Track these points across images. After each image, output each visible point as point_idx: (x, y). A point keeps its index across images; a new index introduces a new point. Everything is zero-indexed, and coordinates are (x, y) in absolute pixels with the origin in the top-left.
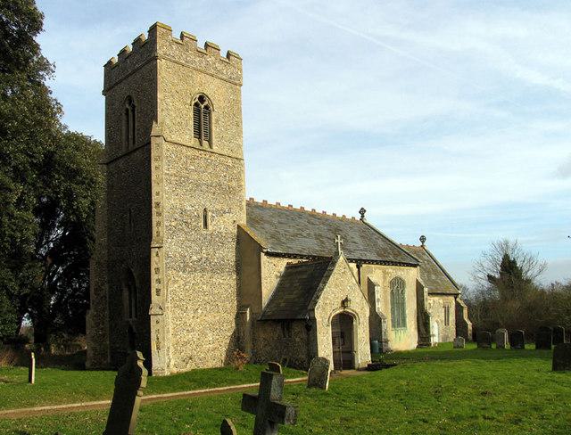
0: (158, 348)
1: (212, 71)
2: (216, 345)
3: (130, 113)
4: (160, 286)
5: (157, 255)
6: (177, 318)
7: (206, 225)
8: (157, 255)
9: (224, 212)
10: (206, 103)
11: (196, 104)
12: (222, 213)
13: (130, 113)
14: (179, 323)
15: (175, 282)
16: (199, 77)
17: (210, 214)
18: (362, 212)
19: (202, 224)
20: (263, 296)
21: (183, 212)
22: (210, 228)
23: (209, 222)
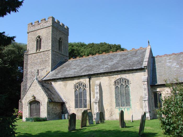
1: (42, 27)
9: (44, 69)
17: (39, 71)
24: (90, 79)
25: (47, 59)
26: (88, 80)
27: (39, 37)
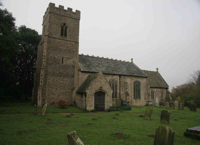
0: (39, 99)
1: (69, 16)
4: (42, 80)
7: (62, 62)
9: (70, 58)
15: (49, 79)
17: (64, 59)
18: (132, 59)
21: (54, 58)
22: (64, 63)
24: (120, 77)
25: (74, 50)
26: (118, 78)
27: (65, 24)
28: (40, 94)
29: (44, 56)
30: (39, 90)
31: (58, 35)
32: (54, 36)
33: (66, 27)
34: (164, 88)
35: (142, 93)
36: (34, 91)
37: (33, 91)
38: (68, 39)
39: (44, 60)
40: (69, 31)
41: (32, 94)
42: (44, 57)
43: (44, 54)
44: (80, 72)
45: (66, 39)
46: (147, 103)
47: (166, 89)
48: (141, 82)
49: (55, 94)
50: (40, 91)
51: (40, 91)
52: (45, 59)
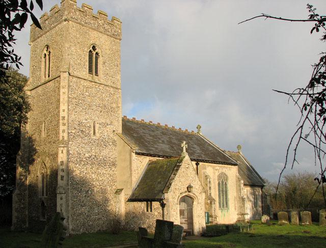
2: (100, 216)
3: (47, 57)
5: (62, 152)
6: (74, 196)
7: (94, 133)
8: (62, 152)
9: (108, 125)
10: (96, 51)
11: (90, 51)
12: (105, 125)
13: (47, 57)
14: (75, 200)
16: (94, 34)
19: (92, 132)
20: (133, 182)
22: (97, 135)
23: (97, 131)
26: (260, 189)
27: (94, 48)
28: (61, 205)
29: (64, 118)
30: (58, 196)
31: (84, 73)
32: (76, 73)
33: (97, 54)
34: (258, 186)
35: (232, 194)
36: (17, 199)
37: (260, 203)
38: (102, 81)
39: (62, 128)
40: (104, 63)
41: (13, 205)
42: (61, 121)
43: (62, 114)
44: (134, 155)
45: (99, 80)
46: (240, 216)
47: (262, 189)
48: (228, 175)
49: (85, 205)
50: (61, 199)
51: (61, 199)
52: (64, 124)
